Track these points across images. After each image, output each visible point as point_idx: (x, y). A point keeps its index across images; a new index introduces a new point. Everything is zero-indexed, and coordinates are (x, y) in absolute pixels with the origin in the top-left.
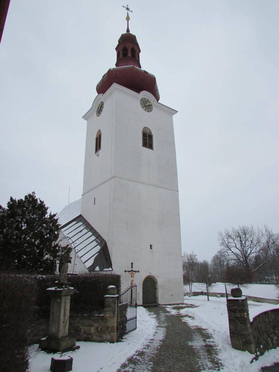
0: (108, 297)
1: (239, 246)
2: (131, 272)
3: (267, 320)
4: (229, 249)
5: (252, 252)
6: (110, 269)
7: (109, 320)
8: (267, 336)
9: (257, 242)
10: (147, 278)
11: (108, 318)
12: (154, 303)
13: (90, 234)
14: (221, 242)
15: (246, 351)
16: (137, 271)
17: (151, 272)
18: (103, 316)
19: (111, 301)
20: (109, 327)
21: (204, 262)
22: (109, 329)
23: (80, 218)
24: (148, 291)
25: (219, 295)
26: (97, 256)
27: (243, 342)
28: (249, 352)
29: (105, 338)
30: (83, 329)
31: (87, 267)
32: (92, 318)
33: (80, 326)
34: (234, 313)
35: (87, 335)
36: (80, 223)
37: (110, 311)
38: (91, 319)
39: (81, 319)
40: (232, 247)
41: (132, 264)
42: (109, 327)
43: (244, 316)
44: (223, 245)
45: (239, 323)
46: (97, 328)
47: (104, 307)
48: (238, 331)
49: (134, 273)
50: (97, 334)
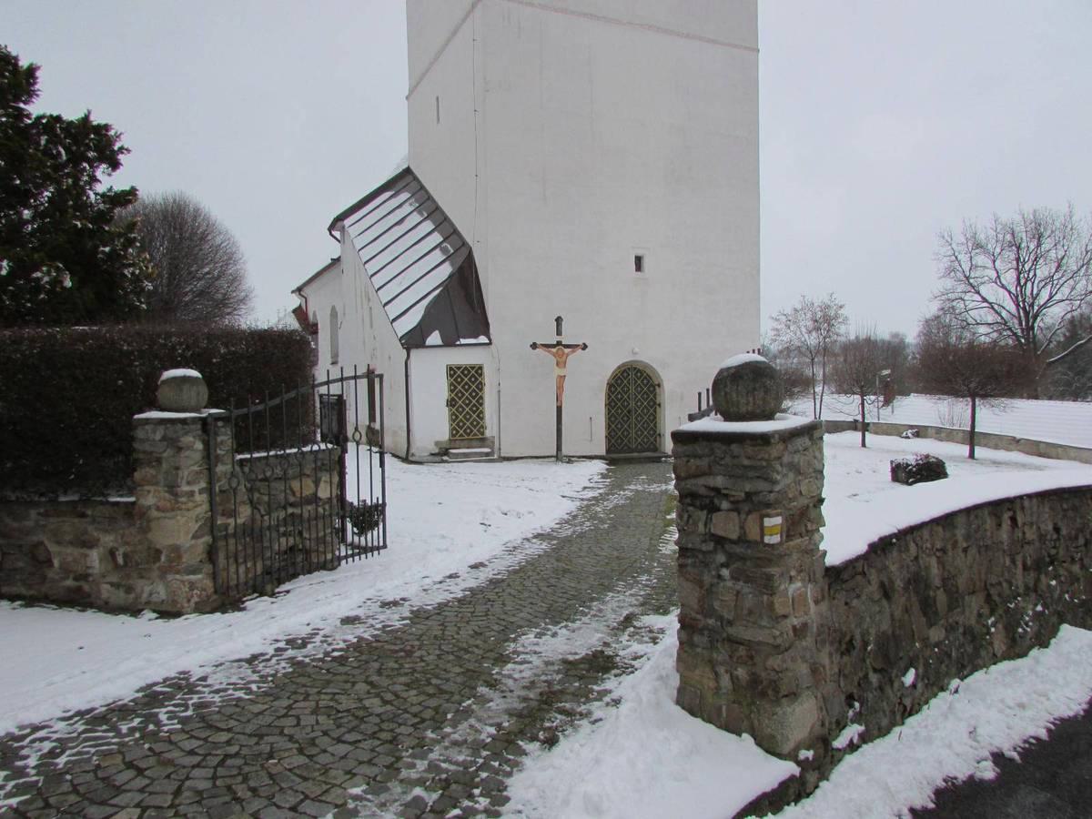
0: (147, 421)
1: (1009, 278)
2: (554, 350)
3: (1004, 534)
4: (973, 287)
5: (1057, 297)
6: (483, 339)
7: (158, 519)
8: (986, 611)
9: (1080, 264)
10: (625, 371)
11: (155, 513)
12: (648, 450)
13: (428, 226)
14: (945, 262)
15: (745, 736)
16: (577, 346)
17: (637, 350)
18: (133, 504)
19: (158, 436)
20: (158, 552)
21: (896, 335)
22: (159, 559)
23: (404, 180)
24: (629, 412)
25: (909, 433)
26: (439, 295)
27: (734, 679)
28: (759, 744)
29: (145, 595)
30: (60, 555)
31: (400, 335)
32: (89, 512)
33: (46, 542)
34: (703, 515)
35: (76, 579)
36: (404, 196)
37: (157, 484)
38: (83, 515)
39: (46, 515)
40: (982, 283)
41: (559, 320)
42: (158, 552)
43: (762, 535)
44: (952, 274)
45: (725, 572)
46: (112, 553)
47: (130, 468)
48: (721, 618)
49: (567, 350)
50: (114, 579)
